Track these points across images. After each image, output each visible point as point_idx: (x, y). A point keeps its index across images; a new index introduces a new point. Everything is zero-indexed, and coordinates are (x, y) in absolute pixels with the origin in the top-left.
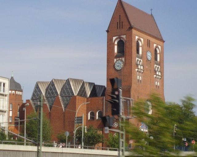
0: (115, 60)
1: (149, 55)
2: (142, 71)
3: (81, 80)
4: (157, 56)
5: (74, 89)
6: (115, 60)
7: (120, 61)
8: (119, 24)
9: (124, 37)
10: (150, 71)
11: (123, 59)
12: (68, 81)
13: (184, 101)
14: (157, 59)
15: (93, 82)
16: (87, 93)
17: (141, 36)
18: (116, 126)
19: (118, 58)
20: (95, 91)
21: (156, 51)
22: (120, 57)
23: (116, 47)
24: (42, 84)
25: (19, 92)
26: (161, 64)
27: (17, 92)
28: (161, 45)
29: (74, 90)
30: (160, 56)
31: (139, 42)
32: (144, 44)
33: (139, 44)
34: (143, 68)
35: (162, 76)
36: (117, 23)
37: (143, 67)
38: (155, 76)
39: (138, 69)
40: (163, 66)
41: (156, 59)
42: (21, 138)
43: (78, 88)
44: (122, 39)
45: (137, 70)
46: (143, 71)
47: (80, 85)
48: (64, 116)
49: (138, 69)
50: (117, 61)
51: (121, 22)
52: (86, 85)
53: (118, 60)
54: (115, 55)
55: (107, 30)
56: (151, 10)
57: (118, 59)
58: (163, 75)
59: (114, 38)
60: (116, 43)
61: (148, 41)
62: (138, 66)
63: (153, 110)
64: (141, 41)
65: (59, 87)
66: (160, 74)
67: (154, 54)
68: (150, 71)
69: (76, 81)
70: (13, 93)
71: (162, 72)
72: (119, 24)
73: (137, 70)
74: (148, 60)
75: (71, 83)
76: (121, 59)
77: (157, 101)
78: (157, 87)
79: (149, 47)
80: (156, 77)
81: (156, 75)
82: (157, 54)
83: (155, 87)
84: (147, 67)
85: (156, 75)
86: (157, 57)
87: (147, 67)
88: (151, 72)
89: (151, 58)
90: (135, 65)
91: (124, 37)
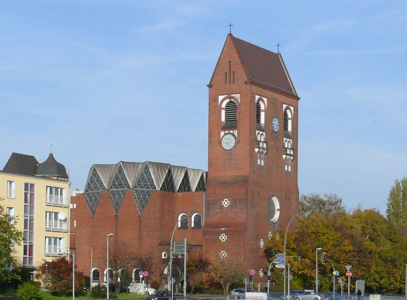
0: (222, 133)
1: (276, 123)
2: (266, 151)
3: (169, 164)
4: (287, 122)
5: (156, 178)
6: (222, 133)
7: (230, 136)
9: (238, 96)
10: (278, 149)
11: (236, 132)
12: (146, 167)
13: (331, 194)
14: (287, 128)
15: (168, 163)
16: (191, 187)
18: (223, 240)
20: (188, 181)
21: (286, 114)
23: (223, 112)
26: (294, 136)
30: (293, 123)
31: (261, 103)
33: (260, 108)
35: (295, 156)
38: (284, 156)
39: (259, 148)
41: (286, 128)
43: (161, 178)
44: (232, 100)
46: (267, 150)
47: (165, 173)
48: (140, 221)
50: (225, 134)
51: (232, 72)
52: (174, 171)
53: (227, 134)
55: (208, 84)
56: (278, 45)
57: (227, 132)
58: (297, 154)
59: (221, 98)
64: (263, 101)
65: (132, 176)
66: (292, 153)
67: (283, 121)
68: (278, 149)
69: (159, 166)
71: (295, 148)
73: (257, 150)
75: (151, 170)
76: (231, 132)
77: (28, 281)
81: (287, 155)
84: (272, 143)
86: (287, 124)
90: (293, 246)
91: (238, 96)
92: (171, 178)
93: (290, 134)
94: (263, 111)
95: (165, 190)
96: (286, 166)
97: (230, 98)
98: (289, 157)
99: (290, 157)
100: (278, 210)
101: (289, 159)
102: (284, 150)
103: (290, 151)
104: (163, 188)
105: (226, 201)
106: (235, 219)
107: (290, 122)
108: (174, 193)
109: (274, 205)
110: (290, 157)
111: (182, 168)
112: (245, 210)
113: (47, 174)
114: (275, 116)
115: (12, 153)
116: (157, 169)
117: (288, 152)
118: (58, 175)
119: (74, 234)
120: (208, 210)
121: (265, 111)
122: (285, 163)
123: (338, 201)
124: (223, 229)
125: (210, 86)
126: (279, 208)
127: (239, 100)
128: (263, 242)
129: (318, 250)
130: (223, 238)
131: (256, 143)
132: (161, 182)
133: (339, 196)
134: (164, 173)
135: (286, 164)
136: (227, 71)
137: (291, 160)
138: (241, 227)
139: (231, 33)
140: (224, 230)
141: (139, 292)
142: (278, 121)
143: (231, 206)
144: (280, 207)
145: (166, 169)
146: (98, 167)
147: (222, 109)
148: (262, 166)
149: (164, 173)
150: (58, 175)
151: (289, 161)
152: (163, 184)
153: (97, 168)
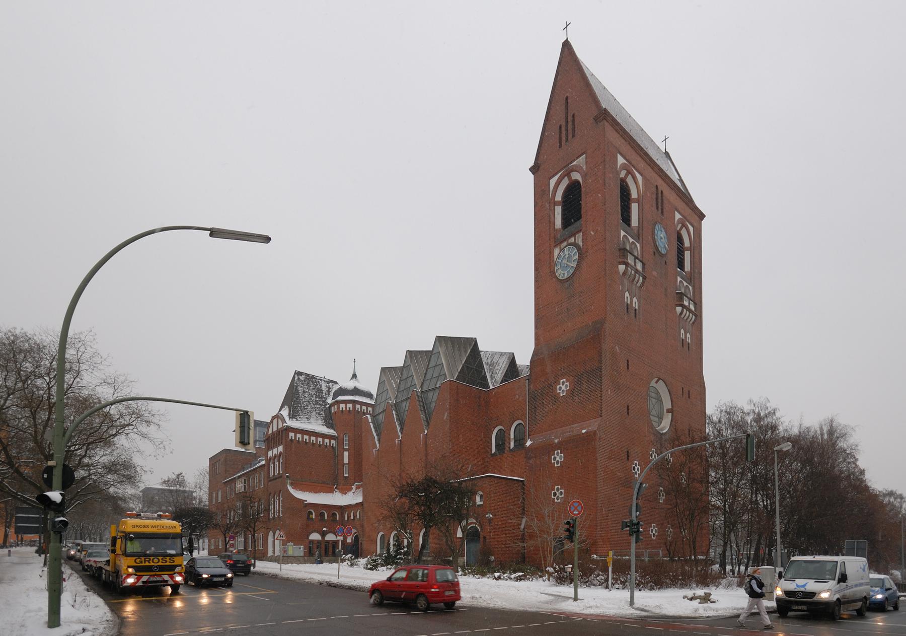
4: (683, 255)
5: (448, 364)
8: (563, 129)
17: (633, 162)
18: (558, 462)
34: (643, 268)
36: (560, 127)
37: (644, 264)
38: (679, 309)
42: (60, 515)
45: (622, 268)
46: (644, 278)
47: (466, 352)
49: (627, 264)
55: (532, 163)
60: (559, 197)
61: (657, 194)
62: (625, 257)
70: (348, 409)
72: (563, 129)
78: (686, 347)
79: (660, 211)
80: (681, 314)
82: (683, 252)
85: (683, 306)
86: (683, 259)
87: (655, 273)
89: (667, 251)
100: (668, 411)
107: (687, 254)
117: (686, 303)
119: (627, 557)
123: (769, 413)
125: (534, 170)
128: (639, 467)
129: (778, 452)
130: (558, 459)
132: (458, 370)
133: (771, 406)
134: (463, 353)
135: (683, 328)
136: (564, 124)
139: (569, 40)
141: (744, 570)
143: (571, 392)
145: (468, 346)
149: (463, 353)
152: (460, 373)
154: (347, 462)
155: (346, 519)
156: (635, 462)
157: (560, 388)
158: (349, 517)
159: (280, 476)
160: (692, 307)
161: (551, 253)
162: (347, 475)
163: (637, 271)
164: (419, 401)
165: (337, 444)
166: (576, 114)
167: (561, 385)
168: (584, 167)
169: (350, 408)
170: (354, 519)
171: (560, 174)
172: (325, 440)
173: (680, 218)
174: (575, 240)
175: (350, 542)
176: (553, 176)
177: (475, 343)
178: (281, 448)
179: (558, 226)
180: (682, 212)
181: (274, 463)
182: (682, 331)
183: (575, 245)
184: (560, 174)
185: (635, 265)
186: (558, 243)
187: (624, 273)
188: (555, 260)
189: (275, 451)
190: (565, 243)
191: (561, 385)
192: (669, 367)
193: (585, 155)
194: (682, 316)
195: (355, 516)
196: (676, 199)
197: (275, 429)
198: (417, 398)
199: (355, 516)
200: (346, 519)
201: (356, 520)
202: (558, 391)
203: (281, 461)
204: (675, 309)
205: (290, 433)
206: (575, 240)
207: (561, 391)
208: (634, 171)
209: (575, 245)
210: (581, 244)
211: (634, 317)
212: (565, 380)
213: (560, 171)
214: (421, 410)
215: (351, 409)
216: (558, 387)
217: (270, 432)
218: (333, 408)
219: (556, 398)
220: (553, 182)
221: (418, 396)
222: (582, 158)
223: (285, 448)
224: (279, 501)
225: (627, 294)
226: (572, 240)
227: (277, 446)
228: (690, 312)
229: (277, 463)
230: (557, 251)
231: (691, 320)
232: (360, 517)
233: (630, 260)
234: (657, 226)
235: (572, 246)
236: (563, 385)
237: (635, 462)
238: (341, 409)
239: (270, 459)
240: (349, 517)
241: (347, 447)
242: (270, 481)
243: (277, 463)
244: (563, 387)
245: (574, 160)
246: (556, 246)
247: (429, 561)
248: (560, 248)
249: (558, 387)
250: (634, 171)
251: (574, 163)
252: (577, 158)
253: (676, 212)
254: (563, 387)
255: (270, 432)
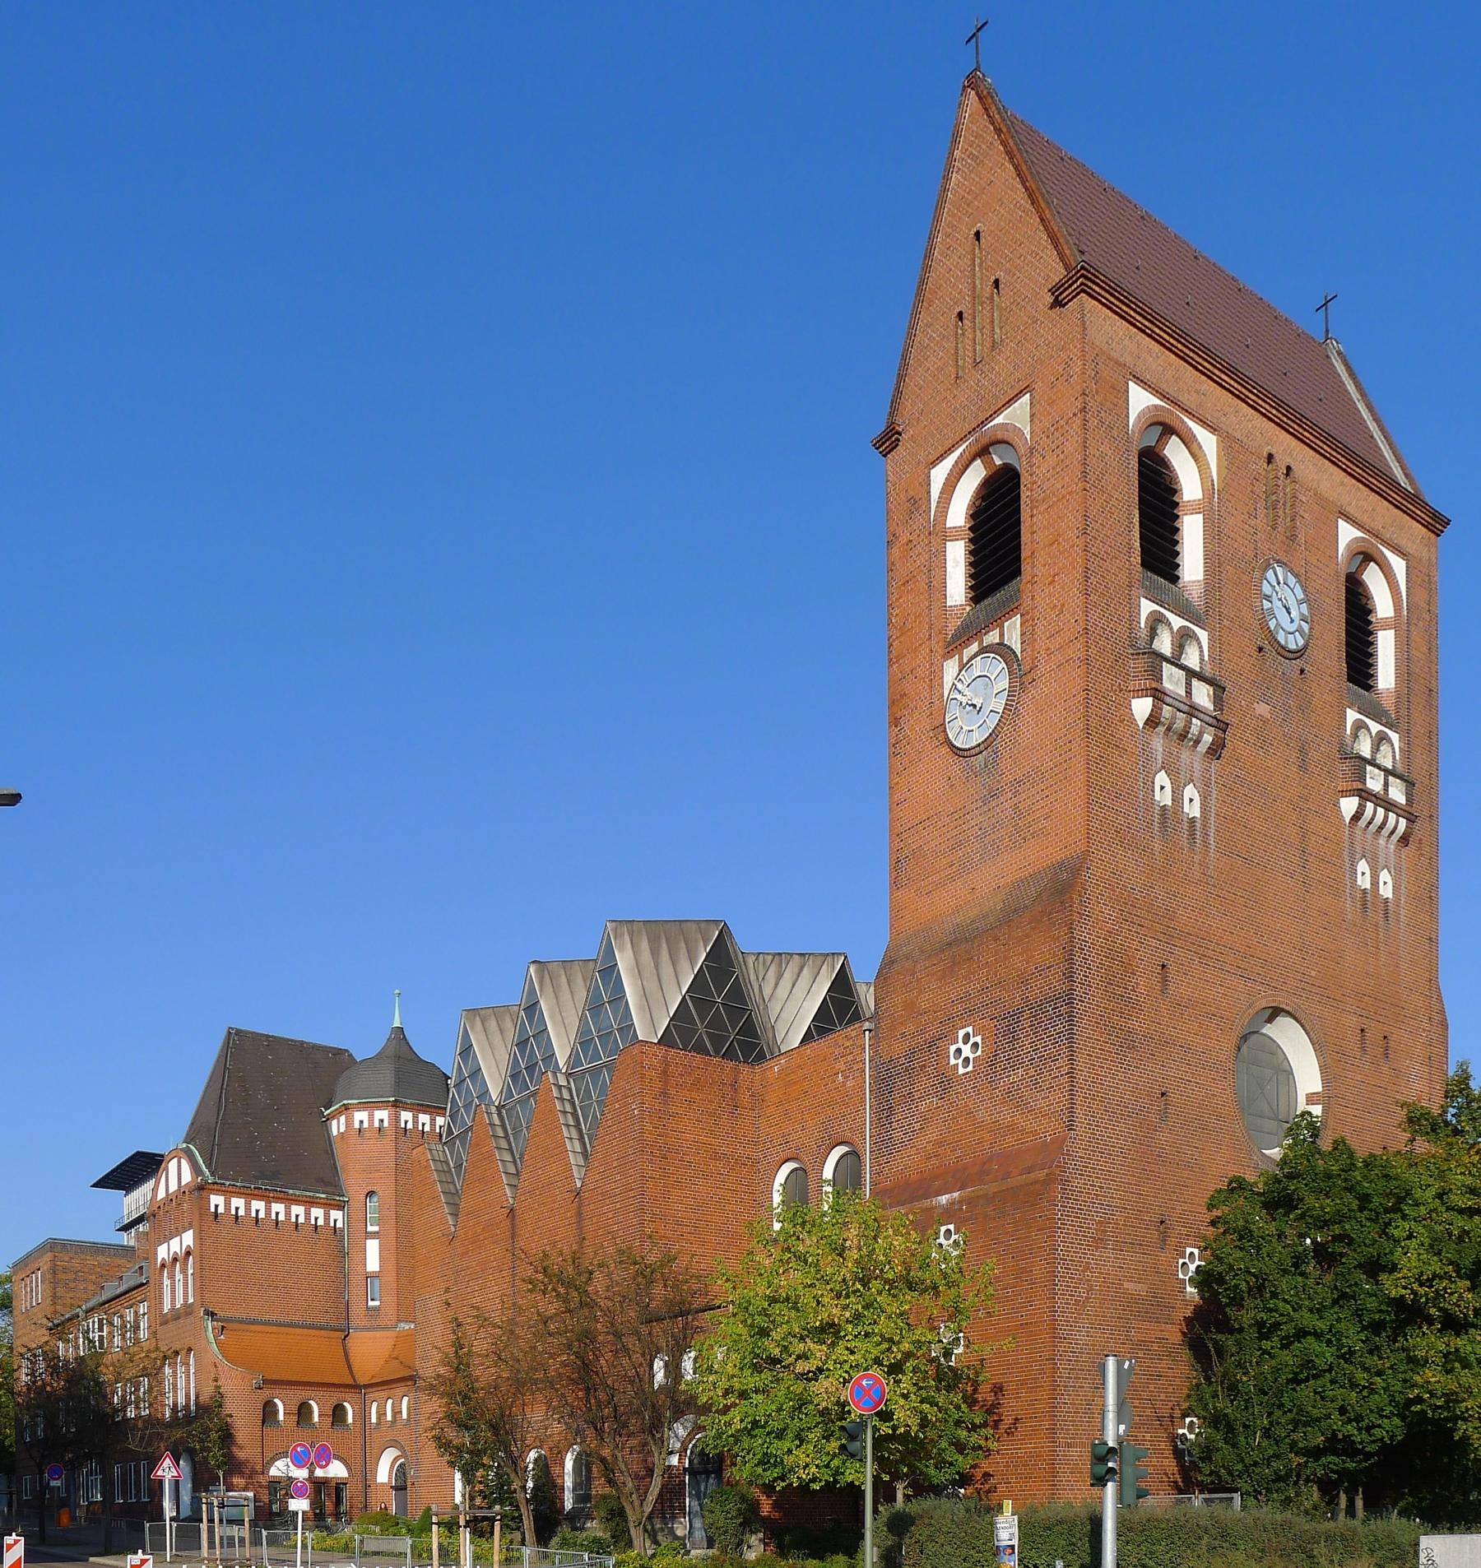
5: (644, 994)
9: (1017, 416)
19: (967, 643)
22: (987, 628)
24: (493, 1025)
25: (424, 1118)
27: (406, 1116)
28: (1411, 548)
29: (640, 1008)
32: (1226, 485)
34: (1218, 701)
38: (1349, 805)
40: (1432, 734)
41: (1360, 668)
47: (692, 961)
49: (1158, 695)
54: (953, 625)
60: (958, 514)
63: (1133, 685)
64: (1189, 441)
70: (376, 1124)
74: (1268, 645)
80: (1357, 817)
81: (1365, 795)
83: (1350, 907)
84: (1262, 709)
85: (1365, 795)
87: (1262, 709)
88: (1303, 767)
92: (738, 994)
93: (1389, 704)
94: (1195, 508)
95: (673, 1046)
96: (1363, 866)
97: (983, 452)
98: (1381, 811)
99: (1386, 818)
101: (1382, 827)
102: (1346, 766)
103: (1386, 784)
104: (680, 1032)
105: (967, 1037)
106: (1012, 1127)
108: (747, 1073)
109: (1290, 1072)
110: (1386, 818)
111: (821, 959)
112: (1063, 1062)
113: (351, 1099)
114: (1281, 556)
115: (223, 1035)
116: (655, 953)
117: (1374, 783)
118: (392, 1099)
120: (884, 1113)
121: (1205, 508)
122: (1358, 849)
124: (944, 1199)
126: (1317, 1086)
127: (1027, 432)
131: (1142, 662)
134: (684, 963)
137: (1395, 838)
138: (1029, 1170)
140: (952, 1203)
142: (1304, 591)
143: (990, 1065)
144: (1325, 1081)
146: (478, 1018)
147: (946, 535)
148: (1193, 820)
149: (684, 963)
150: (392, 1099)
151: (1382, 841)
153: (472, 1027)
154: (377, 1269)
155: (374, 1420)
156: (1189, 1250)
157: (959, 1051)
158: (381, 1414)
159: (188, 1310)
160: (1397, 794)
161: (936, 676)
162: (377, 1303)
163: (1193, 710)
164: (561, 1099)
165: (348, 1220)
166: (1002, 280)
167: (960, 1044)
168: (1027, 432)
169: (382, 1121)
170: (379, 1423)
171: (960, 450)
172: (421, 1116)
173: (1357, 539)
174: (1002, 635)
175: (385, 1480)
176: (941, 457)
177: (721, 933)
178: (188, 1238)
179: (956, 598)
180: (1365, 519)
181: (172, 1277)
182: (1363, 866)
183: (1002, 650)
184: (960, 450)
185: (1189, 693)
186: (955, 645)
187: (1153, 721)
188: (946, 695)
189: (175, 1245)
190: (974, 647)
191: (960, 1044)
192: (1313, 974)
193: (1028, 394)
194: (1362, 823)
195: (397, 1413)
196: (1342, 484)
197: (173, 1187)
198: (555, 1093)
199: (397, 1413)
200: (374, 1420)
201: (399, 1425)
202: (953, 1061)
203: (190, 1271)
204: (1337, 805)
205: (212, 1196)
206: (1002, 635)
207: (960, 1061)
208: (1190, 423)
209: (1002, 650)
210: (1016, 646)
211: (1185, 843)
212: (970, 1029)
213: (949, 451)
214: (568, 1126)
215: (386, 1124)
216: (953, 1048)
217: (161, 1194)
218: (334, 1123)
219: (946, 1080)
220: (939, 475)
221: (560, 1087)
222: (1021, 406)
223: (199, 1238)
224: (188, 1377)
225: (1162, 778)
226: (992, 637)
227: (178, 1232)
228: (1387, 810)
229: (179, 1276)
230: (951, 668)
231: (1392, 832)
232: (409, 1415)
233: (1173, 681)
234: (1270, 574)
235: (992, 655)
236: (965, 1043)
237: (1189, 1250)
238: (357, 1125)
239: (163, 1266)
240: (381, 1414)
241: (376, 1229)
242: (165, 1323)
243: (179, 1276)
244: (967, 1051)
245: (997, 412)
246: (948, 655)
247: (36, 1432)
248: (961, 659)
249: (953, 1048)
250: (1190, 423)
251: (999, 420)
252: (1009, 403)
253: (1341, 522)
254: (967, 1051)
255: (161, 1194)
